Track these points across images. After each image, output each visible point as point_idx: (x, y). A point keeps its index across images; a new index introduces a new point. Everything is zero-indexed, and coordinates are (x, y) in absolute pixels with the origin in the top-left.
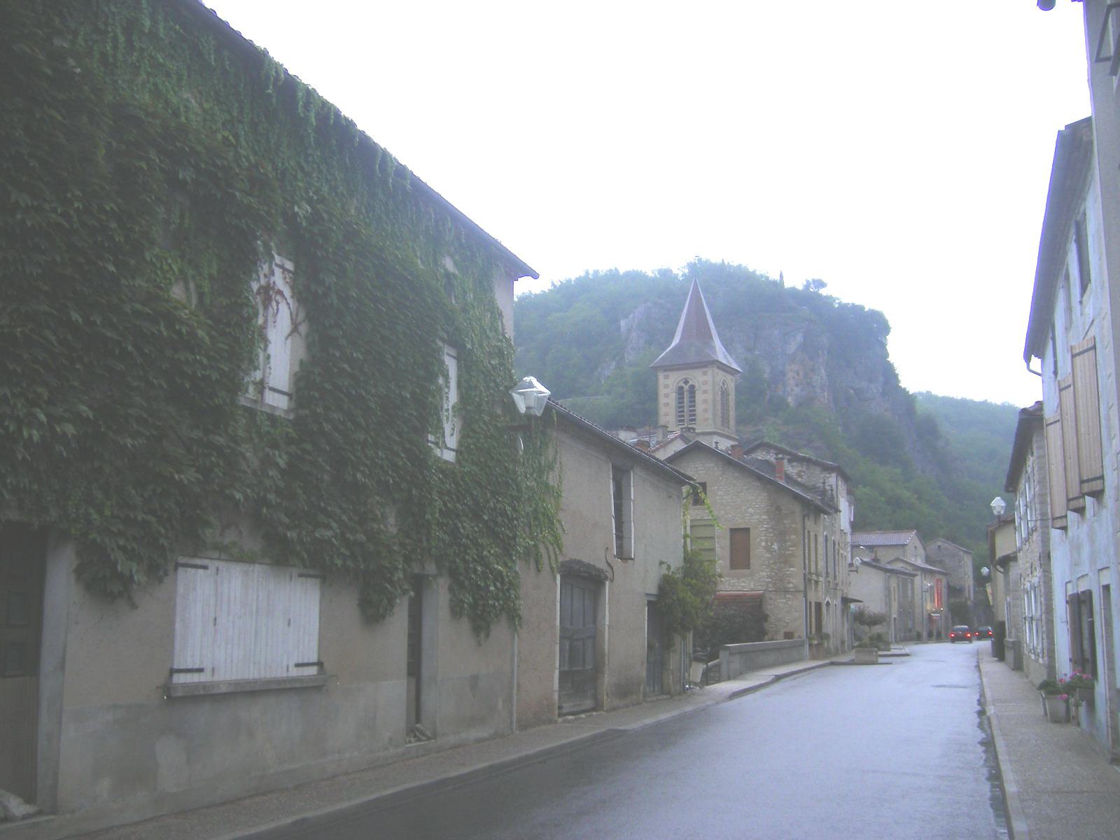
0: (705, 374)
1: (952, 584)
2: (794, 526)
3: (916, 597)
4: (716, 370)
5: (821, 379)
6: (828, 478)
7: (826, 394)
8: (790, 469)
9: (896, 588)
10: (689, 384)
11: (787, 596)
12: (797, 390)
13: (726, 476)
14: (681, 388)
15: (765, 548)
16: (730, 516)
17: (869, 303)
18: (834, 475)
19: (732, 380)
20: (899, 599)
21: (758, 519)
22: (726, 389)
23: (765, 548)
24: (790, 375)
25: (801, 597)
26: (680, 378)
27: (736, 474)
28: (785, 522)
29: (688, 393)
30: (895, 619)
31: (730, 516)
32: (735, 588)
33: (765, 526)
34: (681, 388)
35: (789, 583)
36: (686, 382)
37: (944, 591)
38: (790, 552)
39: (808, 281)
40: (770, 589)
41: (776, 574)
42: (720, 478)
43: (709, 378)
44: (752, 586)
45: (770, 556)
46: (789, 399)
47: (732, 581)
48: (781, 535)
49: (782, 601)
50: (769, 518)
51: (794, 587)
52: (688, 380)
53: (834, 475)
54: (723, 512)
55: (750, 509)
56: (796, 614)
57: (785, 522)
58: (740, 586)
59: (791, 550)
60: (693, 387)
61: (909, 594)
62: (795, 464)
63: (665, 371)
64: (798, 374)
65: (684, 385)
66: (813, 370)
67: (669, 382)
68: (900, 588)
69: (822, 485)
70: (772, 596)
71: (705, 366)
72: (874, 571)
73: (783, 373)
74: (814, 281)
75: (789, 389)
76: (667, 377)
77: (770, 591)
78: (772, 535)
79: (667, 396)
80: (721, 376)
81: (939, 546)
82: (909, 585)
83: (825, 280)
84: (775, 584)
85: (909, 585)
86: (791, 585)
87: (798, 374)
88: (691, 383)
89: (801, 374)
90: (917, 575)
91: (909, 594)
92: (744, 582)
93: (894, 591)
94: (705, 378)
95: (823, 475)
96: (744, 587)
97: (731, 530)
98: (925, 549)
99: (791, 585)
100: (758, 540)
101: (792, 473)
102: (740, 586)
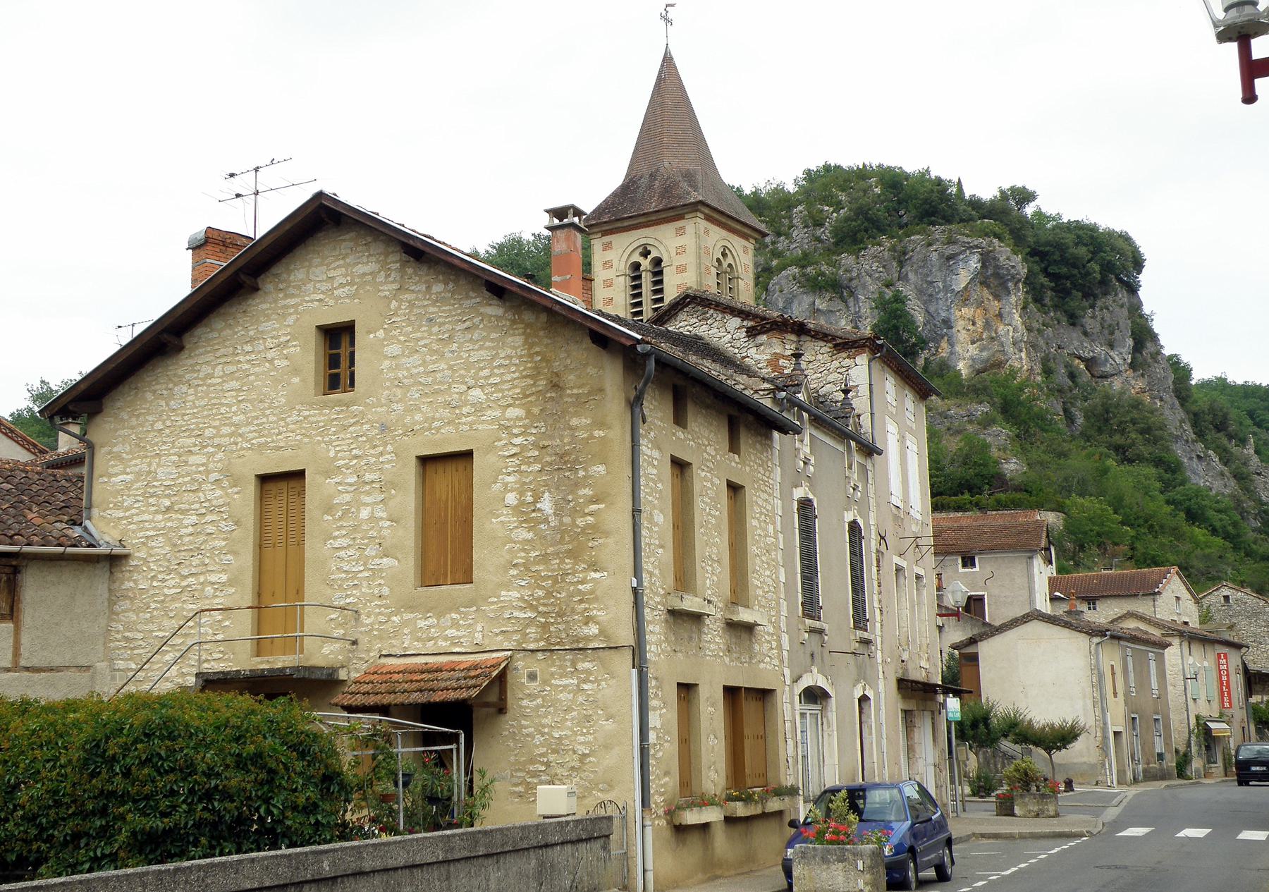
0: (680, 232)
1: (1251, 667)
2: (597, 433)
3: (1170, 688)
4: (703, 224)
5: (1015, 330)
6: (849, 368)
7: (1023, 355)
8: (753, 351)
9: (1118, 670)
10: (650, 257)
11: (580, 666)
12: (973, 350)
13: (407, 296)
14: (636, 266)
15: (515, 508)
16: (418, 417)
17: (1107, 219)
18: (862, 359)
19: (745, 250)
20: (1127, 694)
21: (496, 419)
22: (730, 266)
23: (517, 510)
24: (960, 325)
25: (623, 662)
26: (631, 249)
27: (438, 288)
28: (574, 422)
29: (649, 274)
30: (1116, 734)
31: (418, 417)
32: (430, 647)
33: (517, 441)
34: (636, 266)
35: (588, 620)
36: (646, 253)
37: (1237, 681)
38: (590, 519)
39: (1002, 192)
40: (532, 646)
41: (549, 594)
42: (394, 304)
43: (688, 240)
44: (478, 637)
45: (530, 535)
46: (961, 366)
47: (421, 624)
48: (563, 465)
49: (565, 682)
50: (529, 413)
51: (601, 632)
52: (649, 248)
53: (862, 359)
54: (399, 407)
55: (476, 393)
56: (609, 726)
57: (574, 422)
58: (446, 638)
59: (589, 514)
60: (658, 262)
61: (1154, 685)
62: (764, 337)
63: (605, 233)
64: (974, 324)
65: (641, 260)
66: (1000, 316)
67: (611, 255)
68: (1132, 675)
69: (841, 396)
70: (536, 668)
71: (680, 217)
72: (1066, 633)
73: (948, 324)
74: (1013, 189)
75: (958, 348)
76: (608, 247)
77: (532, 651)
78: (537, 467)
79: (608, 284)
80: (717, 237)
81: (1227, 598)
82: (1153, 664)
83: (1030, 188)
84: (545, 626)
85: (1153, 664)
86: (593, 630)
87: (974, 324)
88: (654, 254)
89: (980, 323)
90: (1170, 645)
91: (1154, 685)
92: (455, 624)
93: (1113, 674)
94: (681, 241)
95: (836, 364)
96: (455, 641)
97: (424, 461)
98: (1197, 602)
99: (593, 630)
100: (497, 487)
101: (758, 362)
102: (446, 638)
